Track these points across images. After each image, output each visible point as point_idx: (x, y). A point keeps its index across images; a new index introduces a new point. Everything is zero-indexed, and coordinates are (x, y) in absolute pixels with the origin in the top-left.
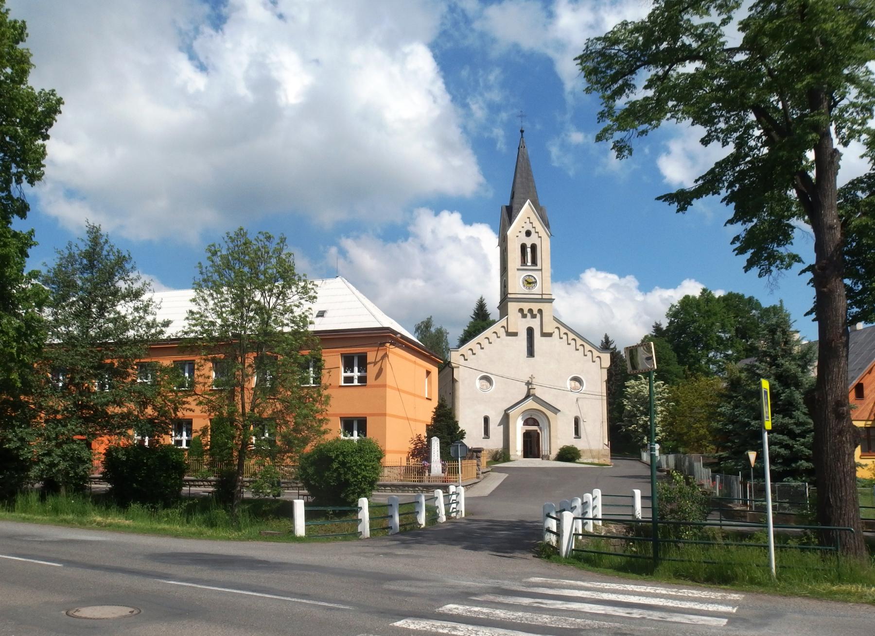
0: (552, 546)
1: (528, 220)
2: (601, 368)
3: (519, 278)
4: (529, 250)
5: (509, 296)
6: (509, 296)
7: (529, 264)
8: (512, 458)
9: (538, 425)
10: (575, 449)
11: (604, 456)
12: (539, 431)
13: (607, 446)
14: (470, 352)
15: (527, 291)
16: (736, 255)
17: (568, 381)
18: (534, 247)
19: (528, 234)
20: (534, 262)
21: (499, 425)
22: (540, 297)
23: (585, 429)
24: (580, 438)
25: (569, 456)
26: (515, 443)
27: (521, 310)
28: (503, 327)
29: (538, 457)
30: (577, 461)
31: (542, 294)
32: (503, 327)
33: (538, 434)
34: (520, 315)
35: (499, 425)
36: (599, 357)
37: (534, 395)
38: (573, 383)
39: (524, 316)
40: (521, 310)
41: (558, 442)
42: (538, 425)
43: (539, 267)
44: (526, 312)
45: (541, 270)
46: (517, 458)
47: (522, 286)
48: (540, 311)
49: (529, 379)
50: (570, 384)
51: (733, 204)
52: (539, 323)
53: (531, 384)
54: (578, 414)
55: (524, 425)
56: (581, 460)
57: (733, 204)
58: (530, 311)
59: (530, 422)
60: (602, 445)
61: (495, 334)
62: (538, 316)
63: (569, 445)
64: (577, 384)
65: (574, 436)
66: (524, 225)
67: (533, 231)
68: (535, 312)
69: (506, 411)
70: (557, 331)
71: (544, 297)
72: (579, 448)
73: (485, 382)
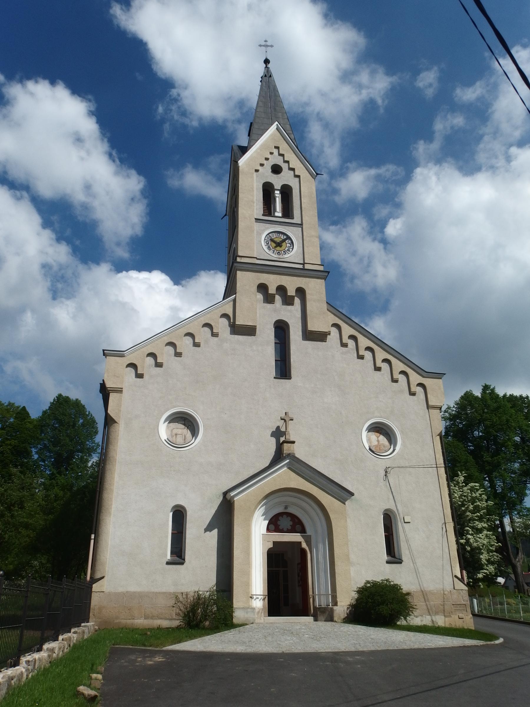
0: (90, 674)
1: (276, 152)
2: (428, 407)
3: (260, 234)
4: (277, 193)
5: (239, 260)
6: (239, 260)
7: (279, 213)
8: (238, 615)
9: (303, 531)
10: (396, 588)
11: (457, 606)
12: (304, 545)
13: (462, 580)
14: (150, 361)
15: (275, 256)
16: (368, 432)
17: (364, 433)
18: (286, 191)
19: (276, 170)
20: (287, 212)
21: (209, 529)
22: (301, 266)
23: (407, 541)
24: (399, 561)
25: (385, 610)
26: (247, 574)
27: (262, 288)
28: (225, 316)
29: (305, 612)
30: (402, 622)
31: (303, 264)
32: (225, 316)
33: (303, 552)
34: (260, 296)
35: (209, 529)
36: (420, 385)
37: (292, 456)
38: (374, 436)
39: (269, 299)
40: (262, 288)
41: (353, 571)
42: (303, 531)
43: (297, 219)
44: (272, 290)
45: (301, 225)
46: (250, 616)
47: (265, 248)
48: (301, 292)
49: (281, 423)
50: (369, 440)
51: (215, 531)
52: (299, 314)
53: (284, 434)
54: (390, 505)
55: (268, 530)
56: (416, 620)
57: (215, 531)
58: (281, 289)
59: (286, 523)
60: (448, 580)
61: (207, 329)
62: (297, 301)
63: (378, 579)
64: (383, 439)
65: (385, 557)
66: (269, 156)
67: (285, 166)
68: (291, 292)
69: (225, 494)
70: (334, 332)
71: (307, 267)
72: (405, 588)
73: (181, 429)
